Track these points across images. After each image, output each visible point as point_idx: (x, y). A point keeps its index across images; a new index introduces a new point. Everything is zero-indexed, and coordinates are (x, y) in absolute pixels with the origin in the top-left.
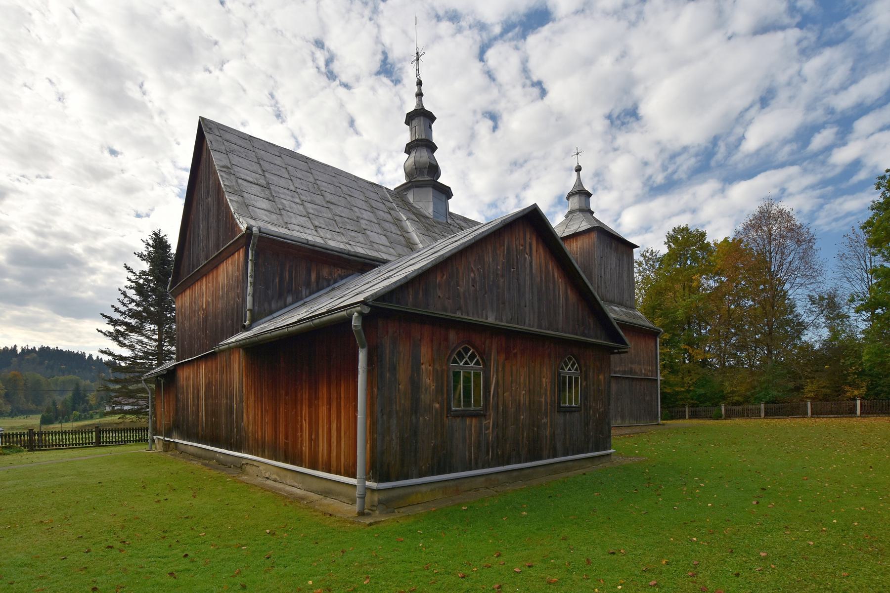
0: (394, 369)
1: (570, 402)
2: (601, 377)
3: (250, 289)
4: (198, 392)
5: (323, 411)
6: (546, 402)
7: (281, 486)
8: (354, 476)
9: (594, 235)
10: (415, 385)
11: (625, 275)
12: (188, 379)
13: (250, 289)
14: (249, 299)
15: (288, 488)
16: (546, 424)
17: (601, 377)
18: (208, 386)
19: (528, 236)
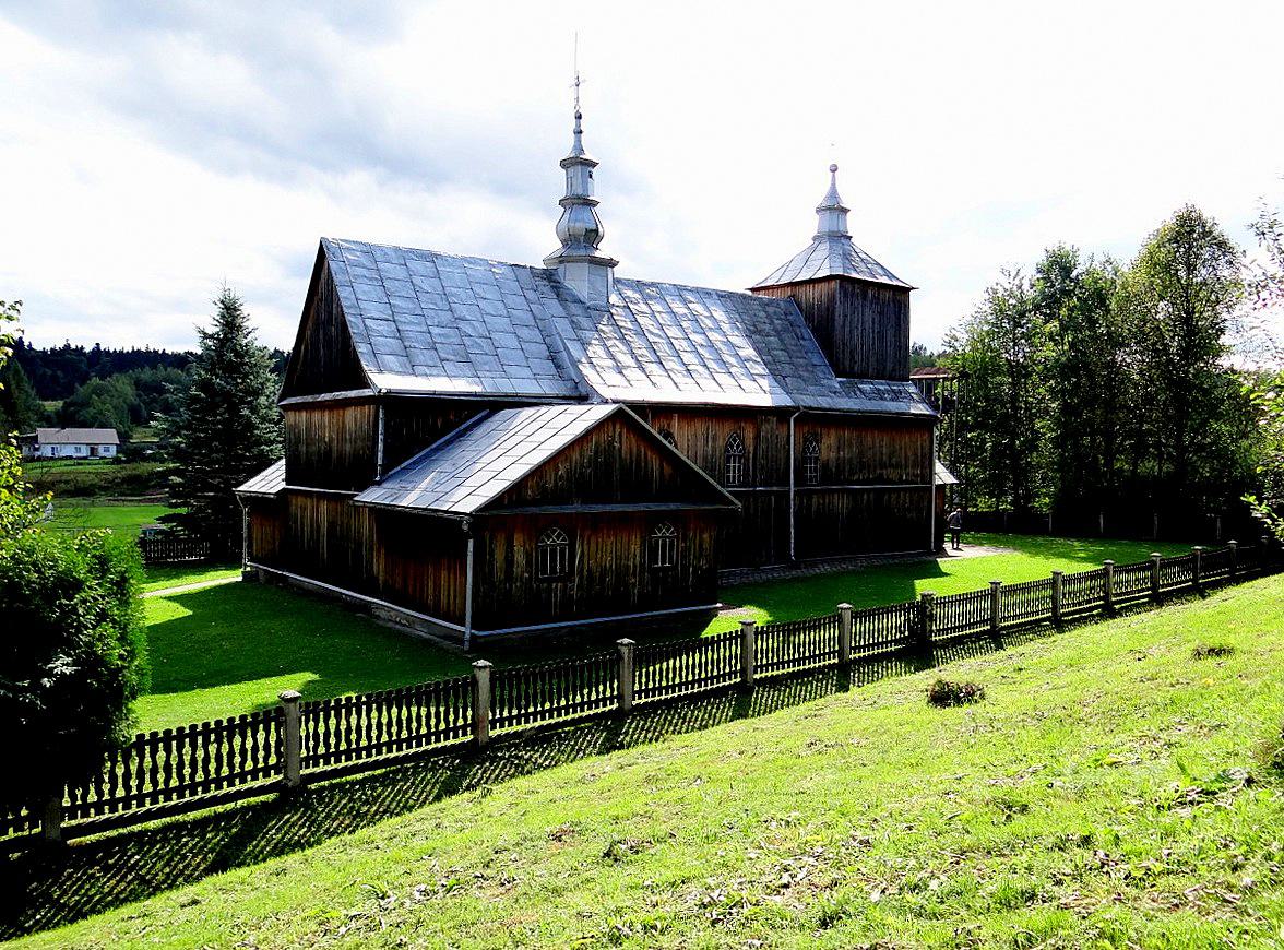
0: (492, 554)
1: (663, 562)
2: (706, 536)
3: (381, 446)
4: (318, 527)
5: (444, 574)
6: (635, 566)
7: (409, 630)
8: (463, 625)
9: (834, 285)
10: (509, 562)
11: (890, 333)
12: (304, 509)
13: (381, 446)
14: (380, 455)
15: (417, 633)
16: (634, 584)
17: (706, 536)
18: (332, 525)
19: (618, 426)
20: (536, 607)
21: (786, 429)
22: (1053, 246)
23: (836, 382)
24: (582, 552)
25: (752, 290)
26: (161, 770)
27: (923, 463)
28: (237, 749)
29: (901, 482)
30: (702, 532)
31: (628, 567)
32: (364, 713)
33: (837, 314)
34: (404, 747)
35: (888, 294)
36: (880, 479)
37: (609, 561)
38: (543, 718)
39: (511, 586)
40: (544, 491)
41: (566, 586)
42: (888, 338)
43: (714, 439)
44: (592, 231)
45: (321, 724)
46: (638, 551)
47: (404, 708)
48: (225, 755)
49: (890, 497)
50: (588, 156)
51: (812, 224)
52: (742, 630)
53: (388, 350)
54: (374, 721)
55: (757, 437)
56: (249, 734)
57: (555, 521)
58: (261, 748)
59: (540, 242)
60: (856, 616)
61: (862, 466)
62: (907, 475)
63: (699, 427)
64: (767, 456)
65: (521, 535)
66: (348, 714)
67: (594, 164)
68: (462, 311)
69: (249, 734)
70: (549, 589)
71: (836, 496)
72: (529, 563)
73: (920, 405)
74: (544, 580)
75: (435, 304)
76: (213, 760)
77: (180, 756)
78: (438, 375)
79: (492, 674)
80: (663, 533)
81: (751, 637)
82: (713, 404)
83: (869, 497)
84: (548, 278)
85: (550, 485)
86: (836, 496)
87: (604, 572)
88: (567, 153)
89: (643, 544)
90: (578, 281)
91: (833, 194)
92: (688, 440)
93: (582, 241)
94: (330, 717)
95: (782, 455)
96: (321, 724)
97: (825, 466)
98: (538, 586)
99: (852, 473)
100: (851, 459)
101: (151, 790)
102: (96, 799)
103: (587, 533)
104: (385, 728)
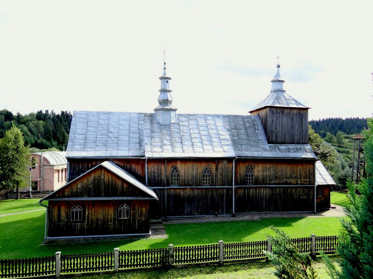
2: (144, 209)
6: (111, 218)
9: (268, 109)
17: (144, 209)
20: (69, 231)
21: (150, 170)
22: (285, 82)
23: (267, 146)
24: (88, 214)
25: (251, 112)
26: (98, 263)
27: (309, 177)
28: (139, 258)
29: (297, 184)
30: (142, 207)
31: (108, 219)
32: (308, 242)
33: (268, 120)
34: (207, 260)
35: (295, 111)
36: (286, 183)
37: (100, 217)
38: (214, 260)
39: (60, 223)
40: (72, 193)
41: (82, 225)
42: (296, 129)
43: (197, 169)
44: (165, 100)
45: (332, 241)
46: (112, 214)
47: (63, 261)
48: (88, 263)
49: (291, 191)
50: (167, 76)
51: (270, 87)
52: (311, 238)
53: (78, 144)
54: (207, 252)
55: (217, 168)
56: (124, 256)
57: (77, 203)
58: (180, 256)
59: (151, 105)
60: (63, 258)
61: (276, 178)
62: (301, 181)
63: (190, 165)
64: (222, 175)
65: (64, 207)
66: (329, 240)
67: (169, 79)
68: (112, 129)
69: (124, 256)
70: (75, 226)
71: (267, 189)
72: (67, 216)
73: (309, 154)
74: (72, 222)
75: (103, 128)
76: (127, 260)
77: (184, 253)
78: (44, 151)
79: (61, 256)
80: (125, 207)
81: (314, 240)
82: (193, 157)
83: (280, 190)
84: (151, 117)
85: (75, 191)
86: (267, 189)
87: (98, 220)
88: (161, 75)
89: (115, 211)
90: (160, 117)
91: (278, 75)
92: (185, 170)
93: (165, 102)
94: (126, 255)
95: (230, 174)
96: (332, 241)
97: (257, 178)
98: (70, 224)
99: (271, 180)
100: (270, 176)
101: (101, 266)
102: (101, 266)
103: (91, 207)
104: (177, 257)
